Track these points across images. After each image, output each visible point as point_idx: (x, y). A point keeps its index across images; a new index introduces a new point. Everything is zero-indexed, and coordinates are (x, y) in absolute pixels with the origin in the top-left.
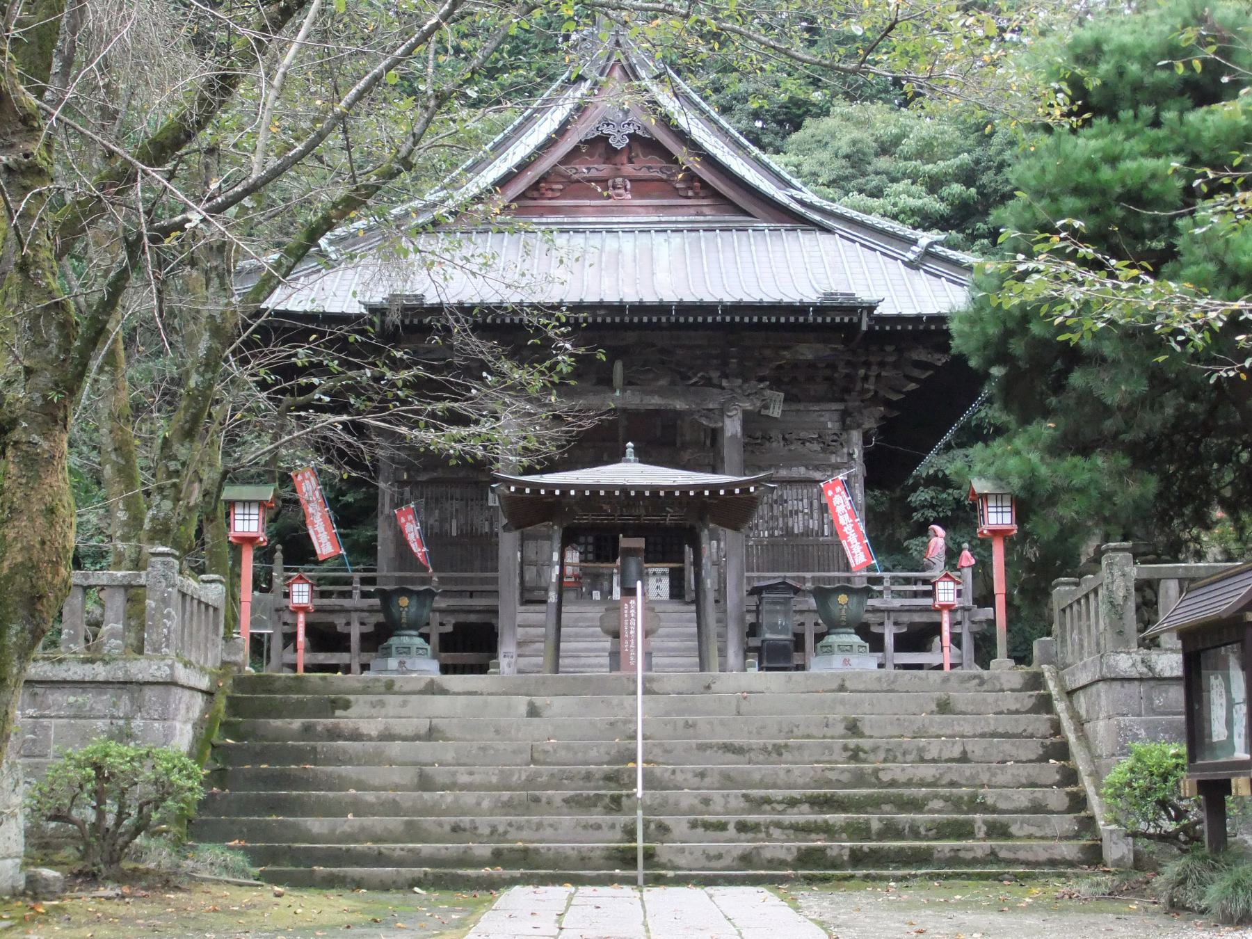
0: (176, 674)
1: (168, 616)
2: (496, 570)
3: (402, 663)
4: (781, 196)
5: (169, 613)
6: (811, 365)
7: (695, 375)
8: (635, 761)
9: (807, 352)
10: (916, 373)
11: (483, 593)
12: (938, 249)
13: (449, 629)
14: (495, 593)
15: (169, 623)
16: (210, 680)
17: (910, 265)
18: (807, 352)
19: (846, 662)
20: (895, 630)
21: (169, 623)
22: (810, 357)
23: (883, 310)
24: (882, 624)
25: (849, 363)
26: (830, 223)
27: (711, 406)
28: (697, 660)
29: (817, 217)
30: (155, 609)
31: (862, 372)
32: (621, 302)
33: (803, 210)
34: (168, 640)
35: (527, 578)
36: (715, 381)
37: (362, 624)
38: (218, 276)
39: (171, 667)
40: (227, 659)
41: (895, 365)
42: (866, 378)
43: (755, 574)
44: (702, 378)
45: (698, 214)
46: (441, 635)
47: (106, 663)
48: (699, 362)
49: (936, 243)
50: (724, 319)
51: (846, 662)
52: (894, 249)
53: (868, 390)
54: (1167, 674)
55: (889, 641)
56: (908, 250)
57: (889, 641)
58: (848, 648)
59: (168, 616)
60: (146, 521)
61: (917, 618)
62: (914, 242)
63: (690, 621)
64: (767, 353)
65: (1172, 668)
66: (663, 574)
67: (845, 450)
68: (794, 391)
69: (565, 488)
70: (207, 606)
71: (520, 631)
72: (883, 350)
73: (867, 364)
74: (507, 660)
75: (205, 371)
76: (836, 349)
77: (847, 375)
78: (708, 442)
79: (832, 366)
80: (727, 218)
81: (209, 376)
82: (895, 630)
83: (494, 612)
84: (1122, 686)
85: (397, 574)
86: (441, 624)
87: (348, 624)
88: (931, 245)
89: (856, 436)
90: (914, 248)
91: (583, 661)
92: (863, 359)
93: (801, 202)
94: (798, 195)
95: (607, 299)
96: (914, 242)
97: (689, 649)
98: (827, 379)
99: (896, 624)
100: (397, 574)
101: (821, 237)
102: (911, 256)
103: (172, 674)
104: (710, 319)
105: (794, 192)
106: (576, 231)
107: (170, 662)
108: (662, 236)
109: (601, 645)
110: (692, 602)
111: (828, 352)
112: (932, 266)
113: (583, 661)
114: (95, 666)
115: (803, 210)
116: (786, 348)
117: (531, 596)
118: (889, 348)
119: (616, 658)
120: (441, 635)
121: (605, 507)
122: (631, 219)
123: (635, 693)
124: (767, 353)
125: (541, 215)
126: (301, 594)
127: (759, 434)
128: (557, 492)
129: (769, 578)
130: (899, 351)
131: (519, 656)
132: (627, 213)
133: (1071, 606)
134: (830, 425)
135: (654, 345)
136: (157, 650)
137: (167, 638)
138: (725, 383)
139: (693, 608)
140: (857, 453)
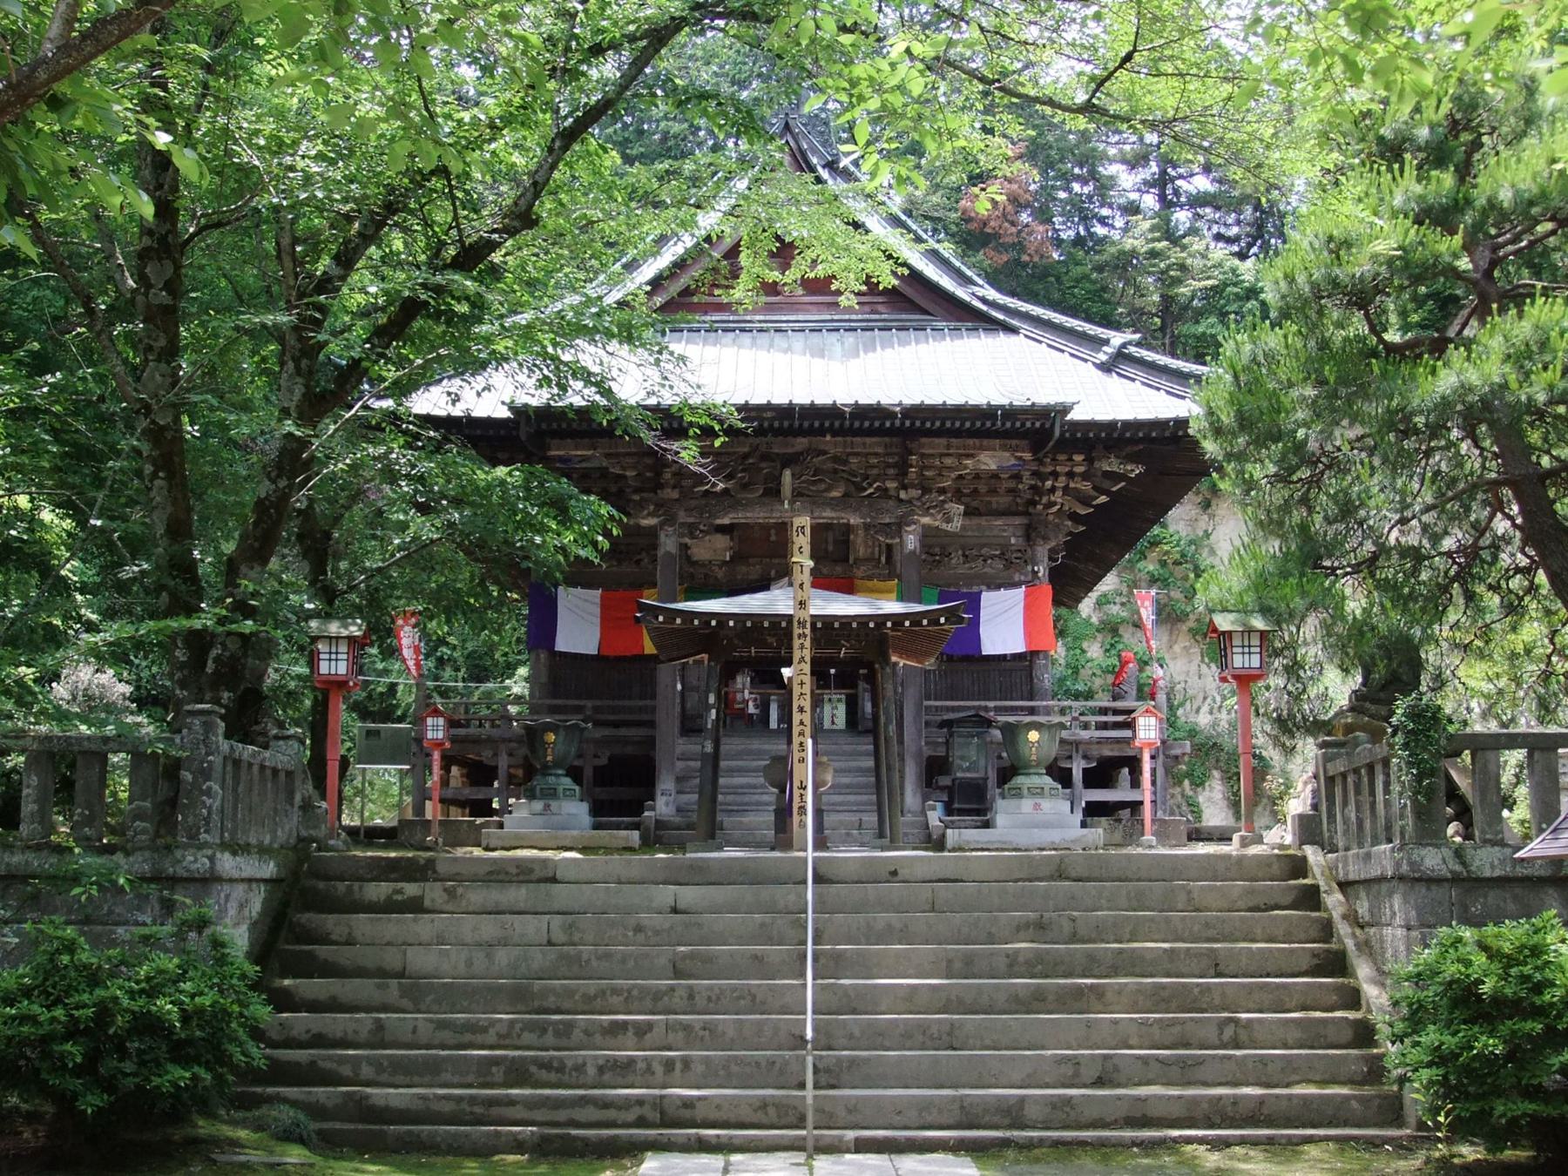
0: (218, 867)
1: (208, 793)
2: (653, 697)
3: (547, 807)
4: (962, 293)
5: (210, 788)
6: (995, 476)
7: (870, 485)
8: (805, 1013)
9: (990, 460)
10: (1106, 484)
11: (639, 724)
12: (1132, 349)
13: (604, 761)
14: (651, 724)
15: (209, 802)
16: (278, 865)
17: (1106, 368)
18: (990, 460)
19: (1037, 806)
20: (1084, 764)
21: (209, 802)
22: (994, 467)
23: (1075, 415)
24: (1070, 757)
25: (1035, 474)
26: (1015, 322)
27: (887, 521)
28: (874, 797)
29: (1001, 316)
30: (192, 784)
31: (1049, 484)
32: (791, 403)
33: (984, 308)
34: (208, 823)
35: (689, 705)
36: (892, 493)
37: (510, 755)
38: (293, 359)
39: (212, 859)
40: (304, 833)
41: (1085, 476)
42: (1053, 490)
43: (932, 703)
44: (877, 489)
45: (873, 312)
46: (595, 768)
47: (127, 854)
48: (875, 471)
49: (1130, 343)
50: (903, 424)
51: (1037, 806)
52: (1084, 352)
53: (1055, 504)
54: (1487, 873)
55: (1077, 775)
56: (1099, 351)
57: (1077, 775)
58: (1038, 792)
59: (208, 793)
60: (210, 662)
61: (1107, 752)
62: (1106, 342)
63: (867, 754)
64: (948, 461)
65: (1493, 867)
66: (839, 700)
67: (1029, 568)
68: (975, 504)
69: (722, 618)
70: (275, 771)
71: (680, 765)
72: (1071, 459)
73: (1055, 475)
74: (664, 798)
75: (278, 476)
76: (1020, 458)
77: (1032, 487)
78: (883, 559)
79: (1017, 477)
80: (904, 316)
81: (283, 483)
82: (1084, 764)
83: (651, 742)
84: (1428, 889)
85: (548, 702)
86: (596, 756)
87: (496, 755)
88: (1124, 345)
89: (1042, 551)
90: (1105, 348)
91: (746, 799)
92: (1049, 469)
93: (984, 300)
94: (980, 292)
95: (775, 401)
96: (1106, 342)
97: (866, 786)
98: (1011, 491)
99: (1085, 757)
100: (548, 702)
101: (1003, 339)
102: (1103, 357)
103: (212, 868)
104: (888, 424)
105: (976, 289)
106: (743, 330)
107: (209, 852)
108: (834, 336)
109: (765, 798)
110: (867, 732)
111: (1013, 461)
112: (1130, 371)
113: (746, 799)
114: (114, 858)
115: (984, 308)
116: (968, 456)
117: (690, 726)
118: (1078, 458)
119: (784, 814)
120: (595, 768)
121: (770, 639)
122: (801, 317)
123: (805, 882)
124: (948, 461)
125: (706, 313)
126: (435, 728)
127: (937, 550)
128: (713, 623)
129: (953, 709)
130: (1090, 460)
131: (678, 792)
132: (797, 311)
133: (1344, 776)
134: (1013, 541)
135: (825, 453)
136: (193, 836)
137: (207, 820)
138: (903, 495)
139: (871, 739)
140: (1042, 570)
